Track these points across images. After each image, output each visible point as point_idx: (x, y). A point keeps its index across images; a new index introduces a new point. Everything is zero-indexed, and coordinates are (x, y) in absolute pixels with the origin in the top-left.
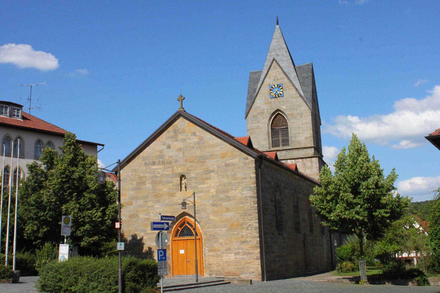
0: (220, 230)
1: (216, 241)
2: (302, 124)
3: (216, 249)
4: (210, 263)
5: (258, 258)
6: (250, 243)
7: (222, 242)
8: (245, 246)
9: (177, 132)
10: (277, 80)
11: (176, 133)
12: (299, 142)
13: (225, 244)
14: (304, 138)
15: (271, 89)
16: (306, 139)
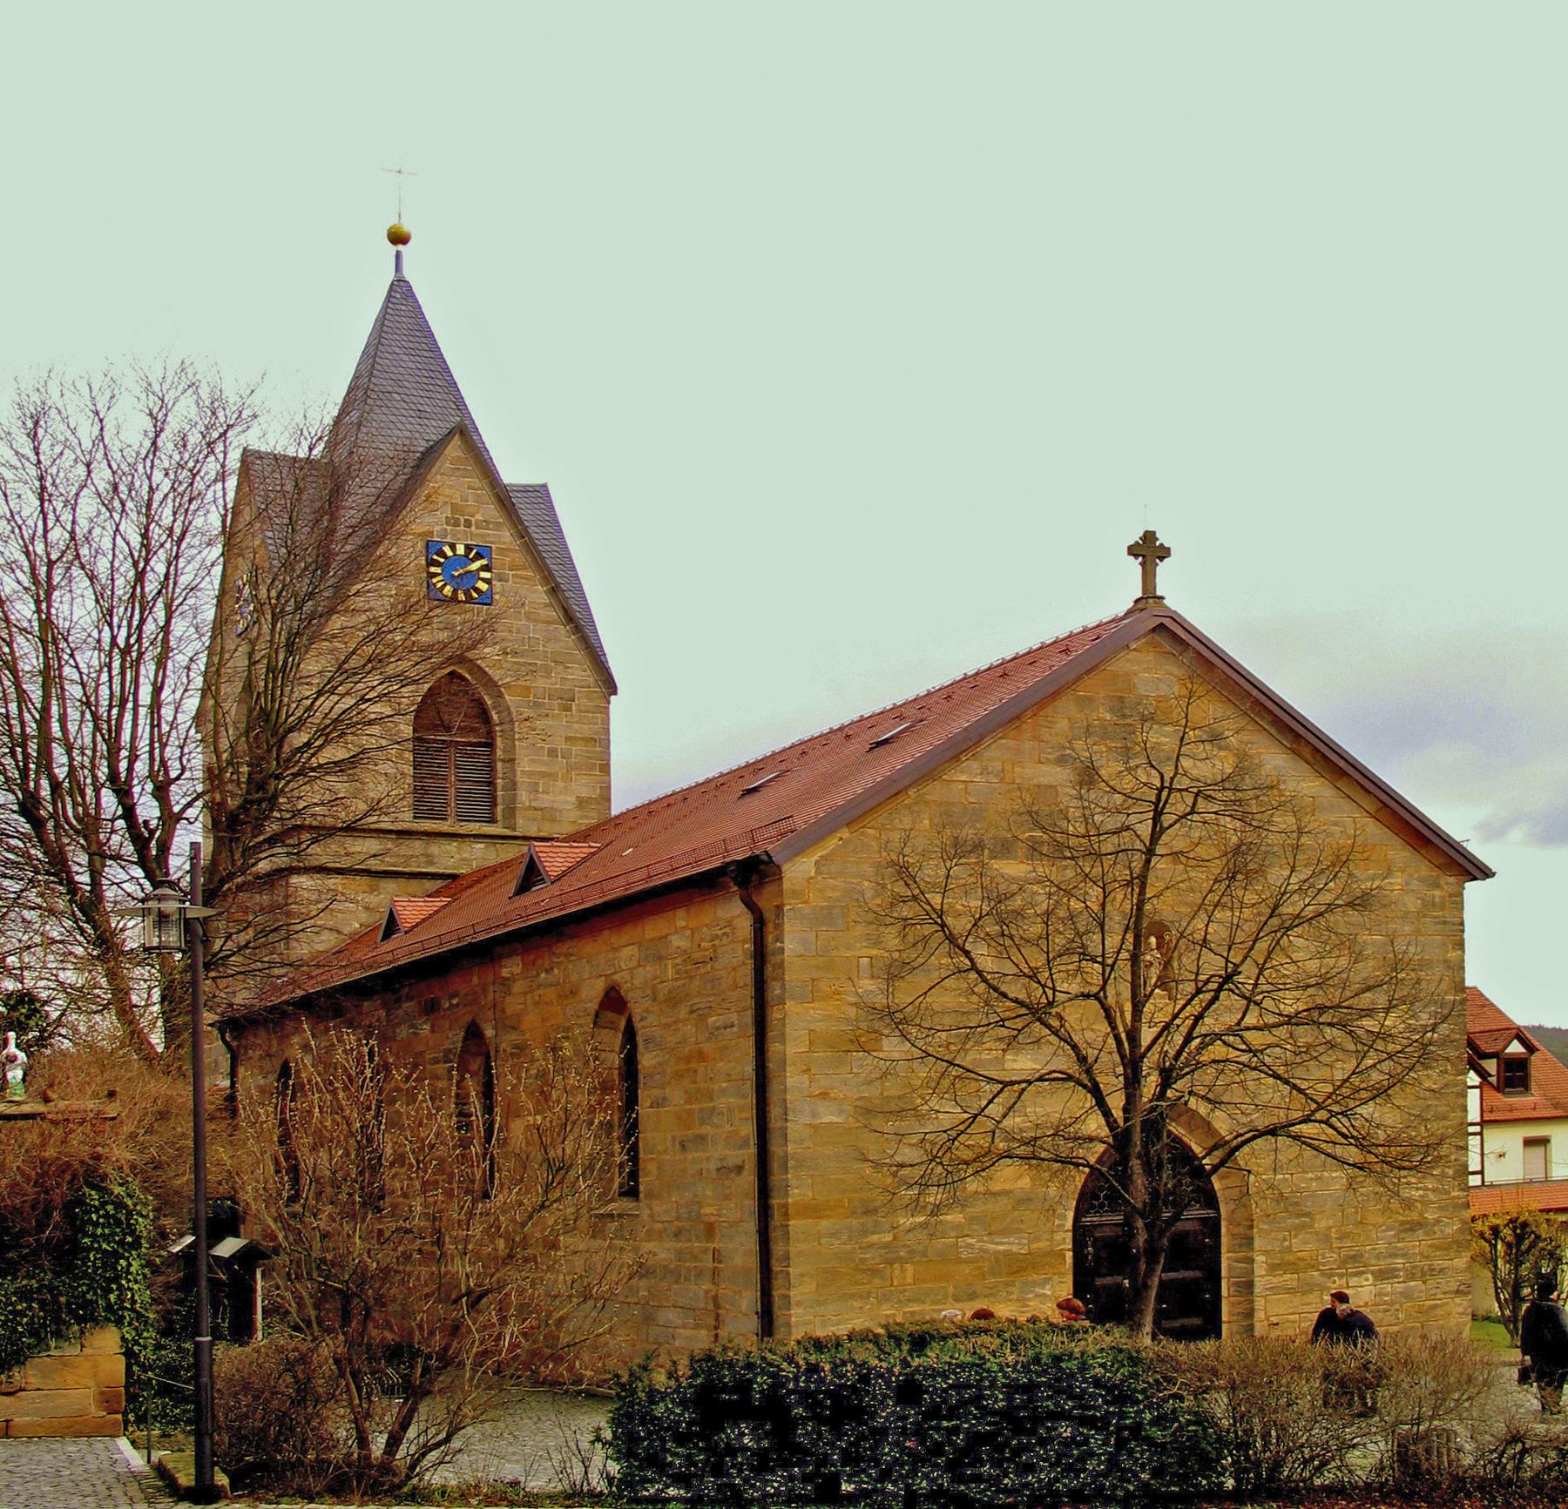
0: (1318, 1179)
1: (1303, 1226)
2: (568, 739)
3: (1302, 1259)
4: (1274, 1320)
5: (1461, 1288)
6: (1436, 1229)
7: (1329, 1228)
8: (1417, 1244)
9: (1127, 711)
10: (468, 524)
11: (1124, 716)
12: (549, 814)
13: (1340, 1238)
14: (572, 799)
15: (435, 557)
16: (580, 803)
